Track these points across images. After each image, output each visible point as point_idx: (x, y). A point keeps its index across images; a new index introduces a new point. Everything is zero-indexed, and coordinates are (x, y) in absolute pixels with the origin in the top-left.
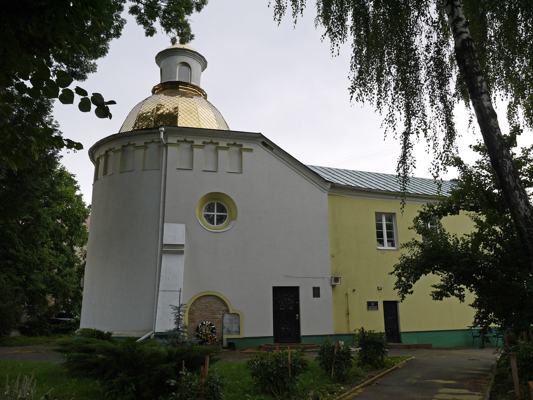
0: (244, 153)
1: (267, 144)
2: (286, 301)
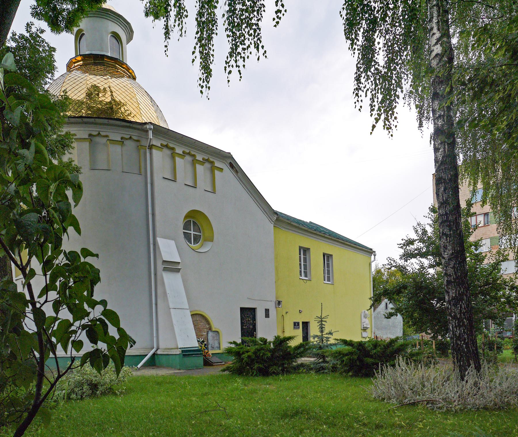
1: (234, 166)
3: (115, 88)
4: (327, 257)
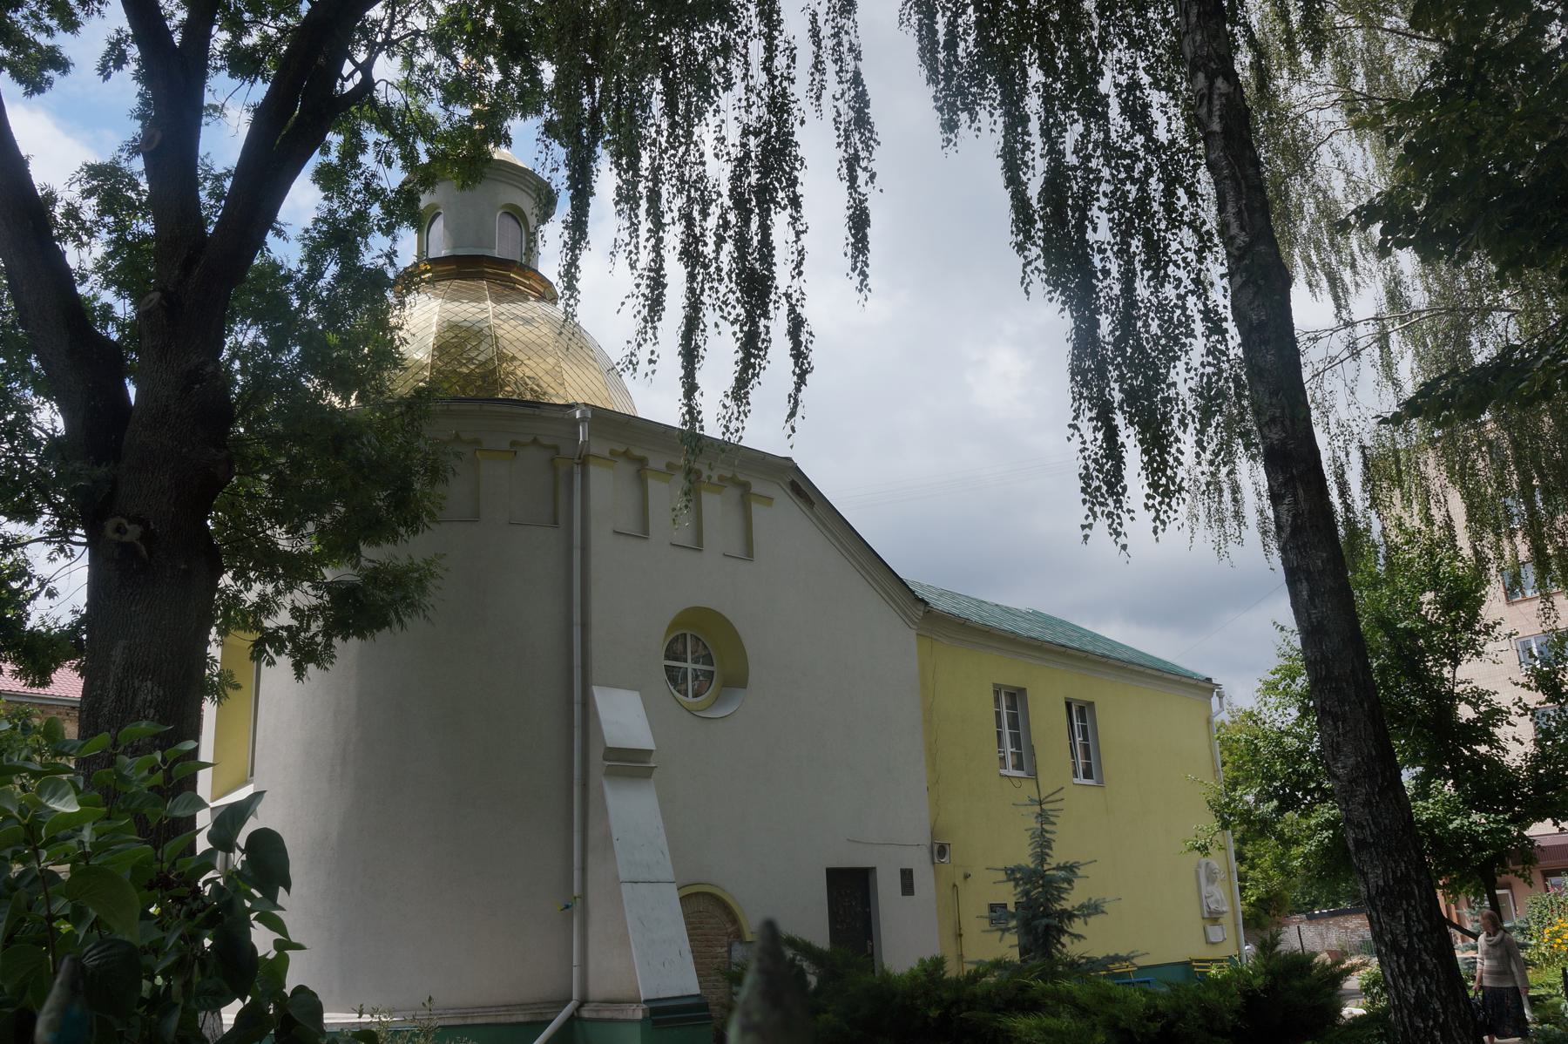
3: (509, 322)
4: (1080, 713)
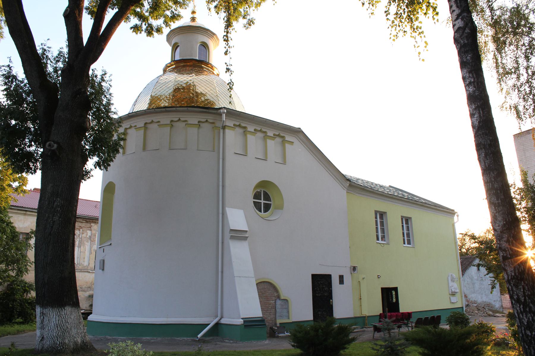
0: (287, 146)
2: (322, 286)
4: (407, 220)
